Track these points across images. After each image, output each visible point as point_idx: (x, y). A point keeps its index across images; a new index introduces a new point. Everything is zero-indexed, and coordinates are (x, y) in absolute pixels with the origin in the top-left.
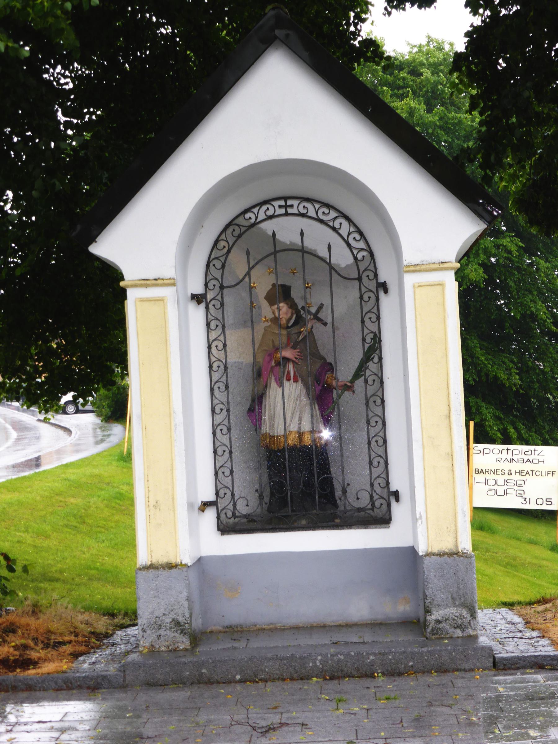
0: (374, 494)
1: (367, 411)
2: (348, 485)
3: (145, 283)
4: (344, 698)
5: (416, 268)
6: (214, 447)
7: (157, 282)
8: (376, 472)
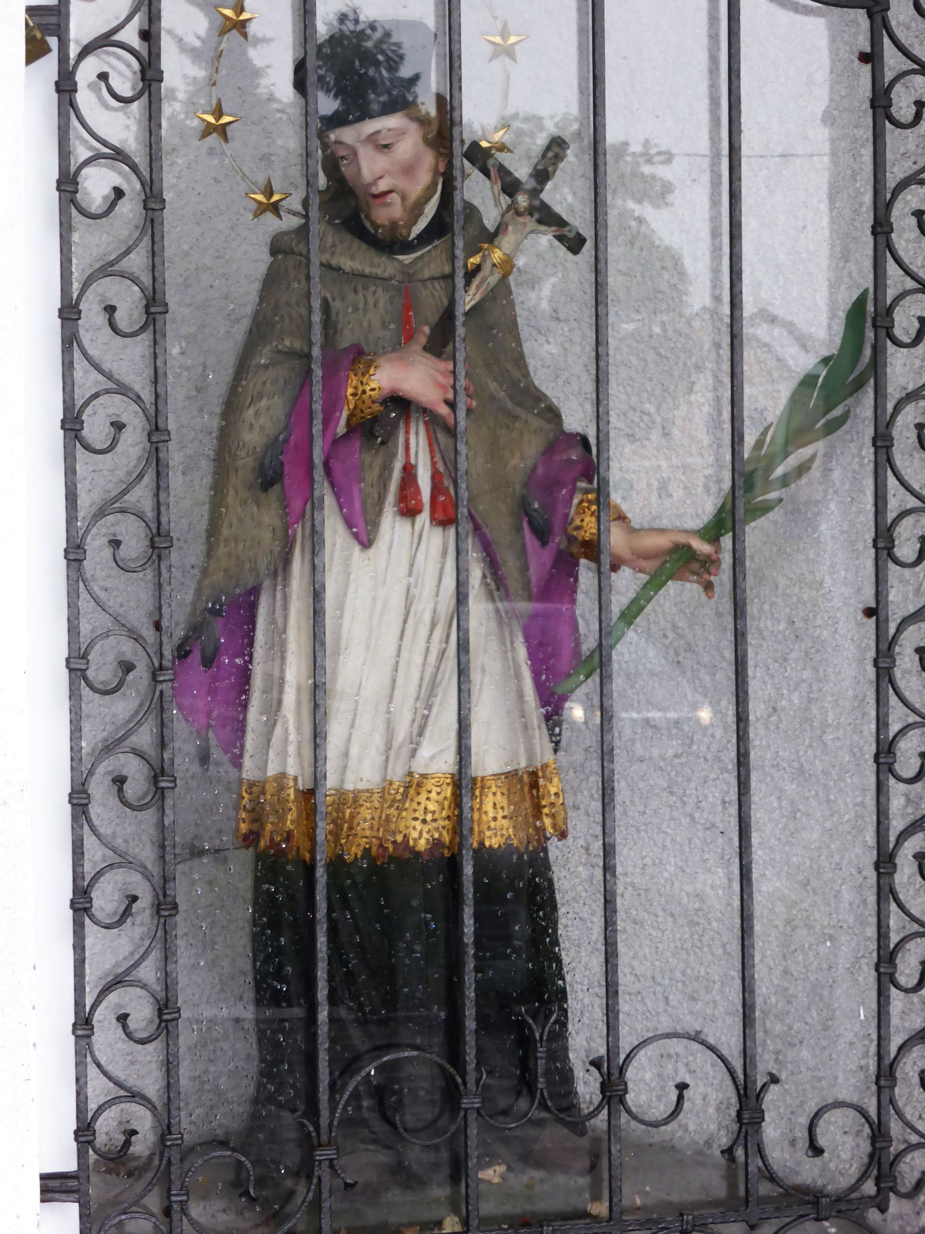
0: (895, 1127)
1: (881, 701)
2: (774, 1080)
6: (77, 876)
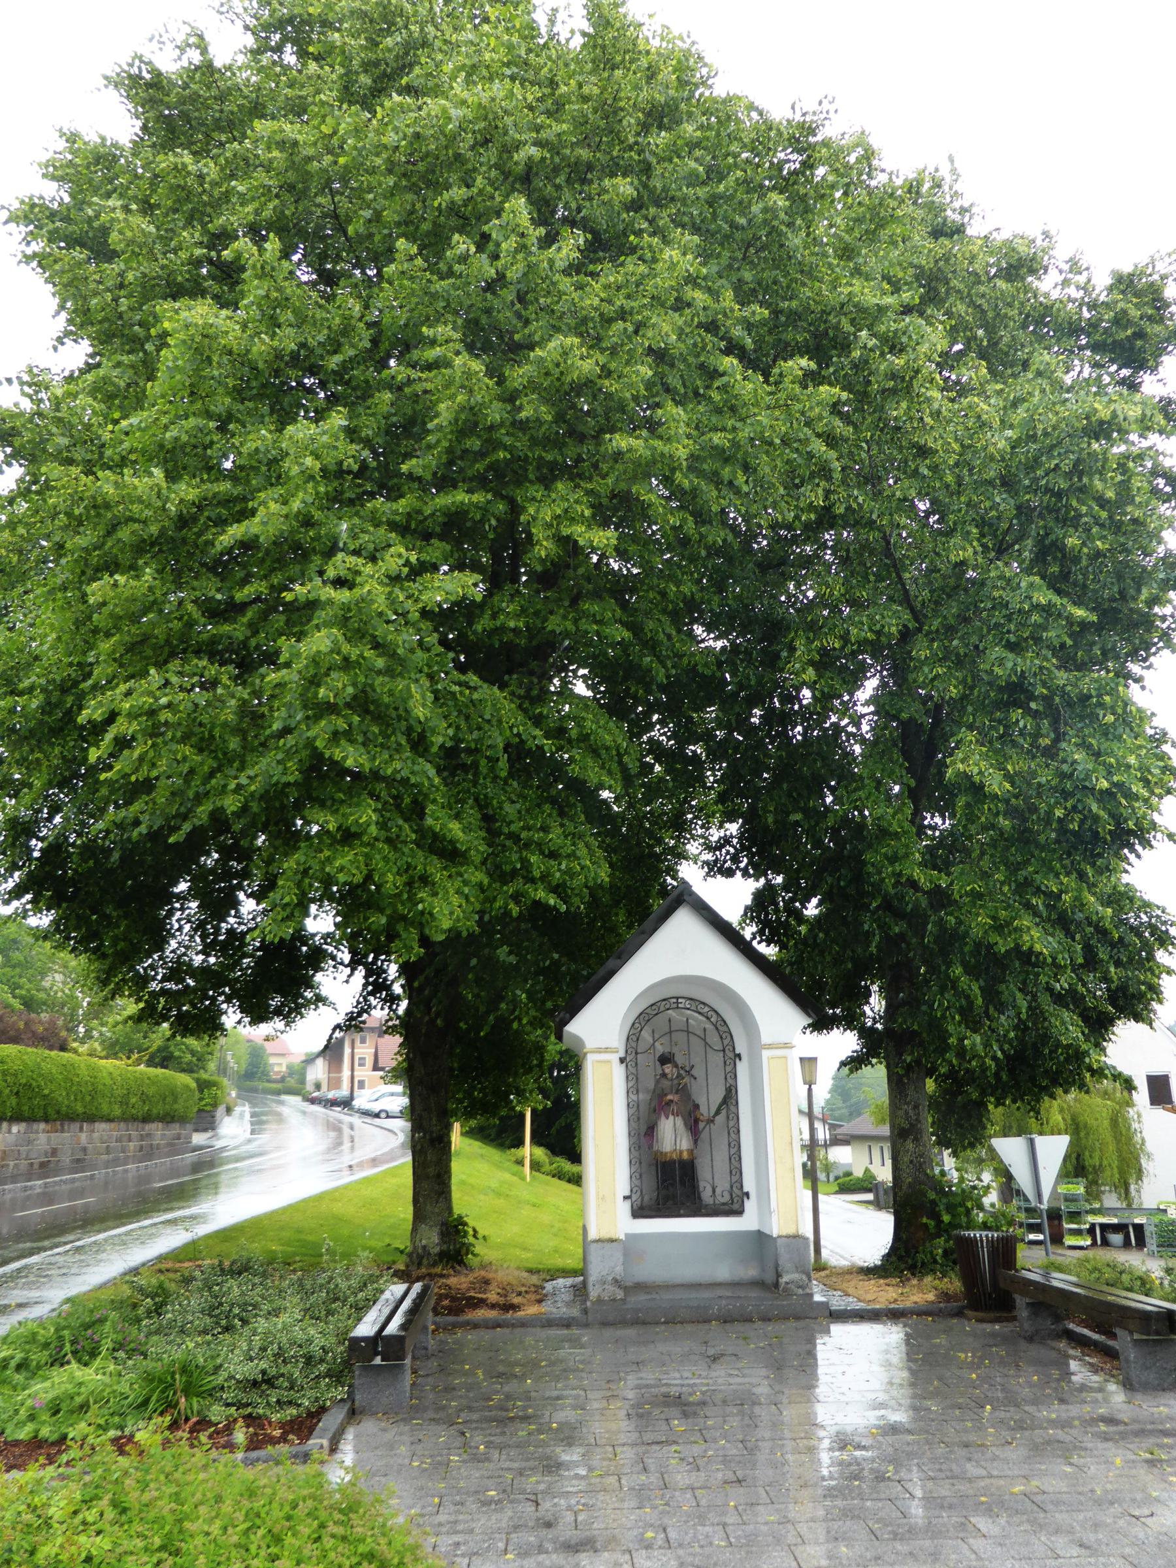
3: (599, 1051)
4: (525, 1275)
5: (770, 1047)
7: (607, 1050)
8: (734, 1179)
